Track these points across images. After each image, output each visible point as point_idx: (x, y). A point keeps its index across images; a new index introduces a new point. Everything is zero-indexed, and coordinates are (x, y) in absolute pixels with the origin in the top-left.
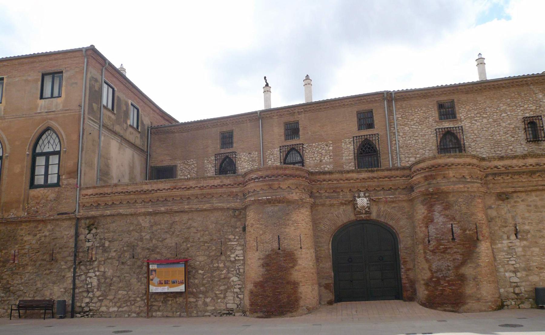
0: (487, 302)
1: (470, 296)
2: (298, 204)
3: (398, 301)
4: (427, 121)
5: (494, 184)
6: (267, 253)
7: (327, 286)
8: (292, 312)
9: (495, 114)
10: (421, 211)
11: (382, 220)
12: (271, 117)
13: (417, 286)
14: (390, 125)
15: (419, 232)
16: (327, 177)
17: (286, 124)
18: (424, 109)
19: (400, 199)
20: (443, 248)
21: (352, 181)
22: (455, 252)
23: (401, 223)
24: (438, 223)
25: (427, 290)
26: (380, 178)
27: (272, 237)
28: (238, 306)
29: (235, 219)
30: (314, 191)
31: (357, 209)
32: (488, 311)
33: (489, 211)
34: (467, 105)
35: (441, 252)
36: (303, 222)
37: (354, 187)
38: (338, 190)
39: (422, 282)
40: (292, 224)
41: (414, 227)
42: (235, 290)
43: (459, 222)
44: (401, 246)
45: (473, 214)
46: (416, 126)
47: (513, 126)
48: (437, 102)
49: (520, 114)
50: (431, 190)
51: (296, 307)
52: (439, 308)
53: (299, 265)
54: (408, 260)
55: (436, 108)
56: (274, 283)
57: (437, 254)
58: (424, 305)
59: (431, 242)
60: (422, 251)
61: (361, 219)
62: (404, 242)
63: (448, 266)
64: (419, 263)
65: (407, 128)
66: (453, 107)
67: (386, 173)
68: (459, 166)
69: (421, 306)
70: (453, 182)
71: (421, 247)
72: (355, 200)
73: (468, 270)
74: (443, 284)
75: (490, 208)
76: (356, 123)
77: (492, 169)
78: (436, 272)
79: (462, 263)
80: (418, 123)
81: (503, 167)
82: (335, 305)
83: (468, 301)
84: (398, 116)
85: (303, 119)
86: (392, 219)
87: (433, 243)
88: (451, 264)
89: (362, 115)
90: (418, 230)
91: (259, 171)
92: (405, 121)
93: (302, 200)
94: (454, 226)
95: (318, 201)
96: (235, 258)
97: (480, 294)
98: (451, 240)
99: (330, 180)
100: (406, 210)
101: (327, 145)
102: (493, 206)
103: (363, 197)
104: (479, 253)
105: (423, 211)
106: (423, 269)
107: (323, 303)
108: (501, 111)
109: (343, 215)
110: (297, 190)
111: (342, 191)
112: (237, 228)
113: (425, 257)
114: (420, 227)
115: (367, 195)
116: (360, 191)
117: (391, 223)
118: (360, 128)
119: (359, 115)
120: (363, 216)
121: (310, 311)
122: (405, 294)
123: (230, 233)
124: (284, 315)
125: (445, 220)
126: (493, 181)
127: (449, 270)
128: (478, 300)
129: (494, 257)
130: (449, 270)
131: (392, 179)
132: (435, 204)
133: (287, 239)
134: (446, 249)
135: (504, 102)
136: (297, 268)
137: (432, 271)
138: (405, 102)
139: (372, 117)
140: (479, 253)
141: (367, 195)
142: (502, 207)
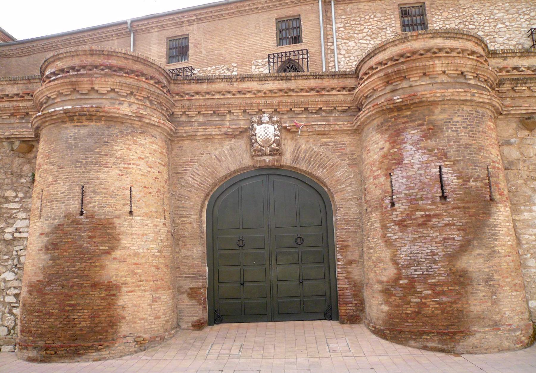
0: (513, 330)
1: (479, 318)
2: (135, 125)
3: (328, 323)
4: (383, 33)
5: (513, 98)
6: (56, 222)
7: (193, 293)
8: (99, 350)
9: (487, 24)
10: (377, 144)
11: (303, 166)
12: (148, 31)
13: (366, 294)
14: (326, 39)
15: (372, 187)
16: (205, 87)
17: (170, 40)
18: (379, 15)
19: (337, 128)
20: (422, 216)
21: (248, 95)
22: (447, 225)
23: (338, 174)
24: (411, 165)
25: (387, 302)
26: (302, 90)
27: (70, 188)
28: (9, 331)
29: (21, 160)
30: (178, 111)
31: (255, 145)
32: (514, 350)
33: (506, 150)
34: (444, 11)
35: (419, 225)
36: (141, 162)
37: (251, 105)
38: (222, 110)
39: (377, 287)
40: (115, 164)
41: (363, 181)
42: (8, 299)
43: (455, 162)
44: (338, 217)
45: (481, 148)
46: (367, 40)
47: (514, 43)
48: (399, 5)
49: (524, 25)
50: (397, 98)
51: (110, 337)
52: (412, 343)
53: (124, 248)
54: (350, 243)
55: (397, 14)
56: (63, 286)
57: (410, 229)
58: (380, 333)
59: (397, 205)
60: (378, 225)
61: (263, 164)
62: (344, 208)
63: (433, 254)
64: (371, 248)
65: (352, 44)
66: (423, 14)
67: (313, 83)
68: (454, 54)
69: (374, 336)
70: (442, 83)
71: (375, 216)
72: (253, 129)
73: (473, 263)
74: (421, 292)
75: (508, 143)
76: (275, 35)
77: (508, 71)
78: (407, 267)
79: (461, 246)
80: (370, 36)
81: (528, 68)
82: (208, 329)
83: (475, 328)
84: (339, 25)
85: (195, 32)
86: (322, 166)
87: (401, 207)
88: (439, 251)
89: (284, 24)
90: (370, 184)
91: (59, 59)
92: (349, 33)
93: (141, 117)
94: (444, 169)
95: (181, 131)
96: (13, 235)
97: (499, 312)
98: (438, 199)
99: (208, 93)
100: (348, 149)
101: (228, 69)
102: (513, 140)
103: (267, 123)
104: (496, 226)
105: (381, 144)
106: (380, 260)
107: (184, 326)
108: (496, 20)
109: (229, 157)
110: (132, 99)
111: (230, 112)
112: (21, 177)
113: (384, 236)
114: (375, 178)
115: (275, 119)
116: (264, 113)
117: (319, 173)
118: (281, 41)
119: (280, 24)
120: (267, 159)
121: (142, 345)
122: (342, 309)
123: (10, 187)
124: (80, 355)
125: (425, 158)
126: (512, 94)
127: (435, 262)
128: (496, 326)
129: (518, 239)
130: (435, 262)
131: (323, 92)
132: (406, 128)
133: (101, 193)
134: (429, 217)
135: (500, 8)
136: (117, 254)
137: (398, 264)
138: (350, 5)
139: (299, 27)
140: (496, 226)
141: (275, 119)
142: (528, 142)
